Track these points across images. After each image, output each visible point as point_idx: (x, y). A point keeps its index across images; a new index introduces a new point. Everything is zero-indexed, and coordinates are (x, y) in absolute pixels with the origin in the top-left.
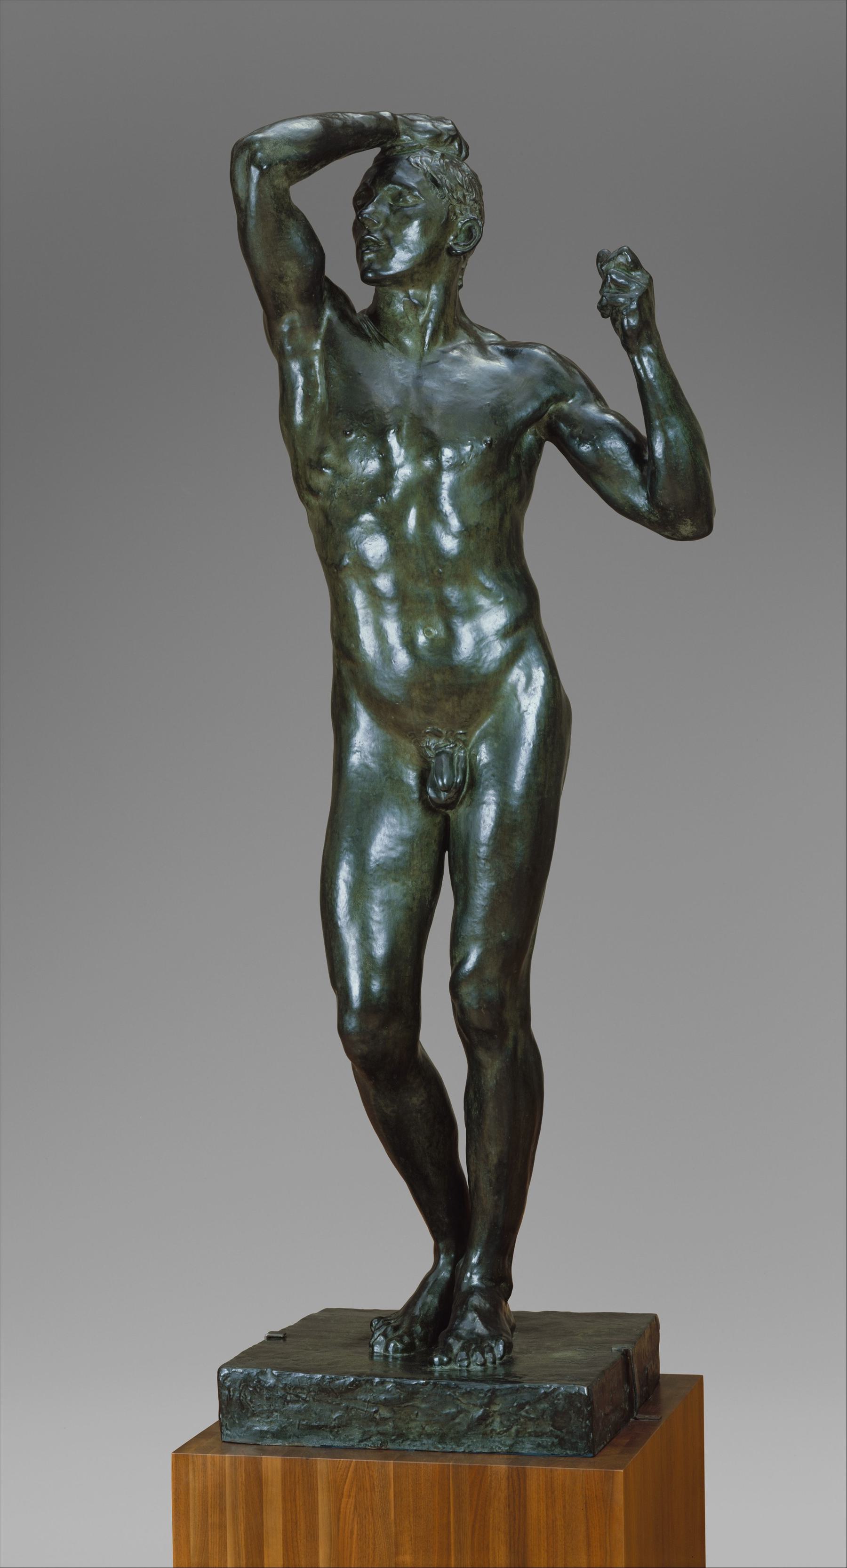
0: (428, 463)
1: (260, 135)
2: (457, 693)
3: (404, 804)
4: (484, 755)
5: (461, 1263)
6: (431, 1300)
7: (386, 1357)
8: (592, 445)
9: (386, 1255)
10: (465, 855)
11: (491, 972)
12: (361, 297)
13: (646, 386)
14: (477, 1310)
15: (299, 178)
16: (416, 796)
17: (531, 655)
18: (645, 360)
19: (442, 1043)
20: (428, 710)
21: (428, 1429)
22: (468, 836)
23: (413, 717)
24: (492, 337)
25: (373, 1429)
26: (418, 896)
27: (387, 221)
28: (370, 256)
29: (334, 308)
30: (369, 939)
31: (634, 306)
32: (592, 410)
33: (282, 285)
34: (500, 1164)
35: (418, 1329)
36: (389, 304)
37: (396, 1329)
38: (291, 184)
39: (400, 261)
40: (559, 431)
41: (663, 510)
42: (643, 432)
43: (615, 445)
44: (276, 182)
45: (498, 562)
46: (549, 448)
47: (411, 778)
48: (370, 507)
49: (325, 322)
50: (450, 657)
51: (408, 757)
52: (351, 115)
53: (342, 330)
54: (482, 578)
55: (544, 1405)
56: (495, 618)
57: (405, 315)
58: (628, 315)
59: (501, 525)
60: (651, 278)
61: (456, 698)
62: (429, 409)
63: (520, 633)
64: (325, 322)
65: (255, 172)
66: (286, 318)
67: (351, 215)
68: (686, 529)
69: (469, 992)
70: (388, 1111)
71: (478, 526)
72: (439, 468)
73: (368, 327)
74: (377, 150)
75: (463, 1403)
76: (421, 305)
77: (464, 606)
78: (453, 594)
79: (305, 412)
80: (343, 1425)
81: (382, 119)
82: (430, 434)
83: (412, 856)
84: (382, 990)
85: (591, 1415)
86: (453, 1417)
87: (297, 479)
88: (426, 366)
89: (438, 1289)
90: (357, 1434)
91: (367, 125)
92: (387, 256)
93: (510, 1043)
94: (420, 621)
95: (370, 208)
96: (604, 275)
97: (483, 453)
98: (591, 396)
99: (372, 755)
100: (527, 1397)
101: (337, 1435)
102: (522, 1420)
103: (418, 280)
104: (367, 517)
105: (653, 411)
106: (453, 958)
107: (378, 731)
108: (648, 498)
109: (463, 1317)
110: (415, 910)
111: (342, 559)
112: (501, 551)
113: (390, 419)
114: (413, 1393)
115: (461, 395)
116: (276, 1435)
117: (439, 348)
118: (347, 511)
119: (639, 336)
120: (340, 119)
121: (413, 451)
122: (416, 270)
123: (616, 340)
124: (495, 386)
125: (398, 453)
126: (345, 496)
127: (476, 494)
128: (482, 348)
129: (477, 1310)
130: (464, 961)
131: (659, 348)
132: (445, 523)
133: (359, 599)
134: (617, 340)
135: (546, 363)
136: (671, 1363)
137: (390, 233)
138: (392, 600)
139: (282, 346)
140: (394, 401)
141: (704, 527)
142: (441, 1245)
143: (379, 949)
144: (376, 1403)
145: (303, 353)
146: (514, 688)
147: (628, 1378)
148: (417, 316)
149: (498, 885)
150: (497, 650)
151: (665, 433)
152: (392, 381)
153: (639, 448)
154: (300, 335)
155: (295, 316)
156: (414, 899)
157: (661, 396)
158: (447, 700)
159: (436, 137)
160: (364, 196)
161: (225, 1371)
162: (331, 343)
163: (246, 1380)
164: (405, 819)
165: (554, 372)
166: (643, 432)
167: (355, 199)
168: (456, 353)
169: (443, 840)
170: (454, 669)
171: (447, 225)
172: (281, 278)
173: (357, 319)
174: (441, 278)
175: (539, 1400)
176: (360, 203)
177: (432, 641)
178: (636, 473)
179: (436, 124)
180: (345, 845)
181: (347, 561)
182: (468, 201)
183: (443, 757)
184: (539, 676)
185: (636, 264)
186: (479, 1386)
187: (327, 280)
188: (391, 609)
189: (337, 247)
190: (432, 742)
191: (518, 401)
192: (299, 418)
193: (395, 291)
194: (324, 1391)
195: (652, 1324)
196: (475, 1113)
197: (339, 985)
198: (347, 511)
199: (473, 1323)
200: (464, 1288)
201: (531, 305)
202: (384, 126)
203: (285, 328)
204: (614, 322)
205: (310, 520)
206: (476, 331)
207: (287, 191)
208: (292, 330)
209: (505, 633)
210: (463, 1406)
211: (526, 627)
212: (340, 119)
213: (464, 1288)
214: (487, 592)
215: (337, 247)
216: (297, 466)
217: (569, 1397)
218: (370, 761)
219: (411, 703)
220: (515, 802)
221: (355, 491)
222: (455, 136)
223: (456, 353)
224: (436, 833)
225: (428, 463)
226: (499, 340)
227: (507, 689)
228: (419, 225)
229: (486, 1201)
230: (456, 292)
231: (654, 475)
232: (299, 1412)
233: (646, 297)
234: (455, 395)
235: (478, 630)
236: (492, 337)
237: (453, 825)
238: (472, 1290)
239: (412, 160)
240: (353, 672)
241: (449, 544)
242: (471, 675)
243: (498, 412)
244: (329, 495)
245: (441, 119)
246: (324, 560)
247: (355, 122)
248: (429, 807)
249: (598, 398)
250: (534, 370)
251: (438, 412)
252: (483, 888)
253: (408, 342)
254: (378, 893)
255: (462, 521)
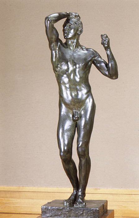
0: (75, 67)
1: (49, 16)
2: (78, 103)
3: (70, 120)
4: (82, 113)
5: (78, 192)
6: (73, 197)
7: (66, 206)
8: (100, 64)
10: (79, 128)
11: (83, 146)
12: (64, 41)
13: (108, 56)
14: (80, 198)
15: (55, 23)
16: (72, 119)
17: (90, 97)
18: (108, 51)
19: (75, 158)
20: (74, 105)
21: (74, 215)
22: (80, 125)
23: (72, 106)
25: (65, 215)
27: (68, 29)
28: (65, 35)
29: (60, 43)
30: (64, 141)
31: (107, 43)
32: (100, 59)
34: (84, 176)
35: (71, 201)
36: (68, 42)
37: (68, 201)
38: (54, 23)
39: (70, 36)
40: (94, 62)
41: (111, 75)
42: (108, 63)
43: (103, 64)
45: (85, 82)
46: (93, 64)
47: (71, 116)
48: (66, 74)
49: (59, 45)
50: (78, 97)
51: (71, 113)
53: (61, 46)
54: (83, 85)
55: (91, 211)
56: (84, 91)
57: (71, 44)
58: (106, 45)
59: (86, 77)
60: (109, 39)
61: (78, 104)
62: (75, 59)
63: (88, 94)
64: (59, 45)
65: (49, 22)
66: (53, 44)
67: (62, 28)
68: (114, 78)
69: (80, 149)
70: (67, 168)
71: (82, 77)
72: (76, 68)
73: (65, 45)
74: (66, 18)
75: (79, 211)
76: (74, 42)
77: (80, 89)
78: (78, 87)
79: (55, 59)
80: (61, 215)
81: (67, 13)
82: (75, 62)
83: (71, 128)
84: (67, 149)
85: (99, 213)
86: (78, 213)
87: (54, 69)
88: (74, 52)
89: (74, 196)
90: (63, 216)
92: (68, 35)
93: (86, 157)
94: (73, 92)
95: (66, 27)
96: (102, 38)
97: (83, 66)
98: (99, 57)
99: (65, 112)
100: (89, 210)
101: (60, 216)
104: (65, 75)
105: (109, 59)
106: (77, 144)
107: (66, 109)
108: (108, 73)
109: (78, 199)
111: (61, 82)
112: (85, 81)
113: (69, 60)
114: (72, 210)
116: (50, 216)
117: (76, 49)
118: (62, 74)
119: (107, 48)
121: (72, 65)
123: (104, 48)
125: (70, 66)
126: (61, 72)
127: (82, 72)
128: (83, 49)
129: (80, 198)
130: (79, 144)
131: (110, 50)
132: (77, 76)
133: (63, 88)
134: (104, 48)
135: (93, 52)
136: (109, 208)
137: (69, 31)
138: (69, 88)
139: (52, 49)
140: (69, 57)
141: (117, 77)
142: (74, 189)
143: (66, 143)
144: (66, 211)
145: (55, 50)
146: (87, 102)
147: (104, 209)
148: (73, 44)
149: (85, 133)
150: (85, 96)
151: (111, 63)
152: (69, 54)
153: (107, 65)
154: (55, 47)
155: (54, 44)
157: (110, 57)
159: (76, 16)
160: (64, 26)
161: (42, 207)
162: (59, 48)
163: (46, 208)
164: (70, 122)
165: (94, 53)
166: (108, 63)
167: (63, 26)
168: (78, 50)
169: (76, 126)
170: (78, 99)
171: (77, 30)
172: (52, 38)
173: (63, 44)
174: (76, 38)
175: (91, 210)
176: (64, 26)
177: (75, 95)
178: (106, 69)
180: (61, 126)
181: (62, 82)
183: (76, 113)
184: (91, 100)
185: (107, 37)
186: (82, 209)
187: (59, 39)
188: (68, 90)
189: (61, 33)
190: (74, 110)
191: (88, 57)
192: (54, 60)
193: (69, 40)
194: (58, 210)
195: (107, 201)
196: (80, 168)
197: (60, 148)
198: (62, 74)
199: (80, 200)
200: (78, 195)
201: (90, 41)
203: (52, 46)
204: (103, 45)
205: (56, 76)
207: (53, 25)
208: (53, 46)
209: (86, 94)
211: (89, 93)
213: (78, 195)
214: (83, 87)
215: (61, 33)
217: (95, 210)
218: (65, 114)
219: (71, 104)
220: (87, 120)
221: (63, 71)
222: (78, 16)
223: (78, 50)
224: (75, 125)
225: (75, 67)
227: (86, 102)
229: (82, 182)
231: (109, 69)
232: (54, 213)
233: (108, 42)
235: (82, 93)
237: (77, 123)
238: (80, 195)
240: (62, 99)
241: (78, 79)
242: (81, 100)
243: (85, 59)
244: (59, 72)
245: (76, 13)
246: (58, 82)
248: (74, 120)
249: (101, 57)
250: (90, 52)
251: (76, 59)
252: (82, 133)
253: (71, 48)
254: (66, 134)
255: (80, 76)
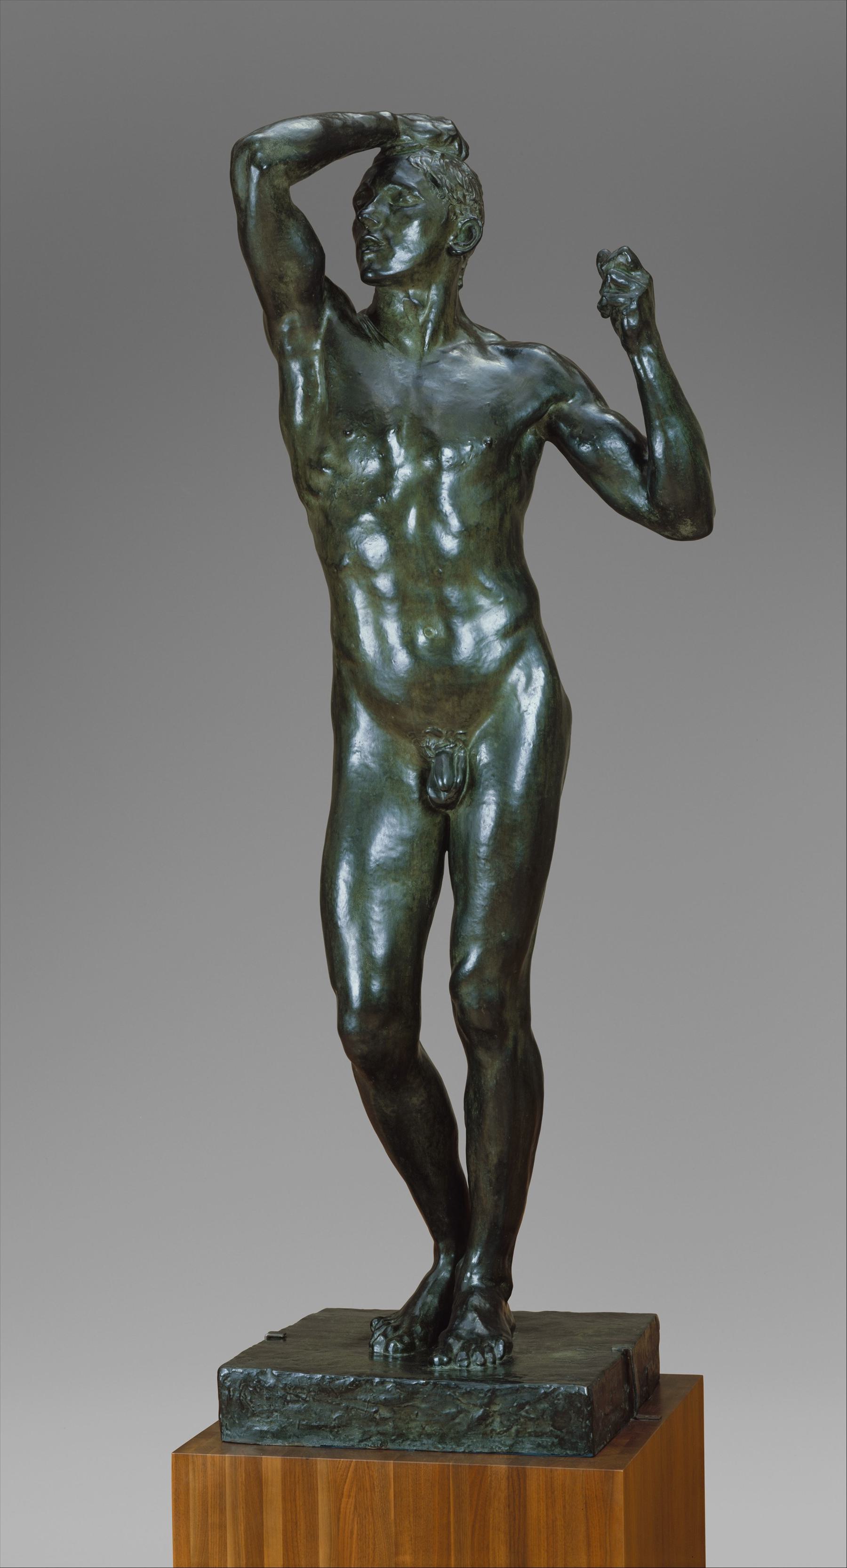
0: (428, 463)
1: (260, 135)
2: (457, 693)
3: (404, 804)
4: (484, 755)
5: (461, 1263)
6: (431, 1300)
7: (386, 1357)
8: (592, 445)
9: (386, 1255)
10: (465, 855)
11: (491, 972)
12: (361, 297)
13: (646, 386)
14: (477, 1310)
15: (299, 178)
16: (416, 796)
17: (531, 655)
18: (645, 360)
19: (442, 1043)
20: (428, 710)
21: (428, 1429)
22: (468, 836)
23: (413, 717)
24: (492, 337)
25: (373, 1429)
26: (418, 896)
27: (387, 221)
28: (370, 256)
29: (334, 308)
30: (369, 939)
31: (634, 306)
32: (592, 410)
33: (282, 285)
34: (500, 1164)
35: (418, 1329)
36: (389, 304)
37: (396, 1329)
38: (291, 184)
39: (400, 261)
40: (559, 431)
41: (663, 510)
42: (643, 432)
43: (615, 445)
44: (276, 182)
45: (498, 562)
46: (549, 448)
47: (411, 778)
48: (370, 507)
49: (325, 322)
50: (450, 657)
51: (408, 757)
52: (351, 115)
53: (342, 330)
54: (482, 578)
55: (544, 1405)
56: (495, 618)
57: (405, 315)
58: (628, 315)
59: (501, 525)
60: (651, 278)
61: (456, 698)
62: (429, 409)
63: (520, 633)
64: (325, 322)
65: (255, 172)
66: (286, 318)
67: (351, 215)
68: (686, 529)
69: (469, 992)
70: (388, 1111)
71: (478, 526)
72: (439, 468)
73: (368, 327)
74: (377, 150)
75: (463, 1403)
76: (421, 305)
77: (464, 606)
78: (453, 594)
79: (305, 412)
80: (343, 1425)
81: (382, 119)
82: (430, 434)
83: (412, 856)
84: (382, 990)
85: (591, 1415)
86: (453, 1417)
87: (297, 479)
88: (426, 366)
89: (438, 1289)
90: (357, 1434)
91: (367, 125)
92: (387, 256)
93: (510, 1043)
94: (420, 621)
95: (370, 208)
96: (604, 275)
97: (483, 453)
98: (591, 396)
99: (372, 755)
100: (527, 1397)
101: (337, 1435)
102: (522, 1420)
103: (418, 280)
104: (367, 517)
105: (653, 411)
106: (453, 958)
107: (378, 731)
108: (648, 498)
109: (463, 1317)
110: (415, 910)
111: (342, 559)
112: (501, 551)
113: (390, 419)
114: (413, 1393)
115: (461, 395)
116: (276, 1435)
117: (439, 348)
118: (347, 511)
119: (639, 336)
120: (340, 119)
121: (413, 451)
122: (416, 270)
123: (616, 340)
124: (495, 386)
125: (398, 453)
126: (345, 496)
127: (476, 494)
128: (482, 348)
129: (477, 1310)
130: (464, 961)
131: (659, 348)
132: (445, 523)
133: (359, 599)
134: (617, 340)
135: (546, 363)
136: (671, 1363)
137: (390, 233)
138: (392, 600)
139: (282, 346)
140: (394, 401)
141: (704, 527)
142: (441, 1245)
143: (379, 949)
144: (376, 1403)
145: (303, 353)
146: (514, 688)
147: (628, 1378)
148: (417, 316)
149: (498, 885)
150: (497, 650)
151: (665, 433)
152: (392, 381)
153: (639, 448)
154: (300, 335)
155: (295, 316)
156: (414, 899)
157: (661, 396)
158: (447, 700)
159: (436, 137)
160: (364, 196)
161: (225, 1371)
162: (331, 343)
163: (246, 1380)
164: (405, 819)
165: (554, 372)
166: (643, 432)
167: (355, 199)
168: (456, 353)
169: (443, 840)
170: (454, 669)
171: (447, 225)
172: (281, 278)
173: (357, 319)
174: (441, 278)
175: (539, 1400)
176: (360, 203)
177: (432, 641)
178: (636, 473)
179: (436, 124)
180: (345, 845)
181: (347, 561)
182: (468, 201)
183: (443, 757)
184: (539, 676)
185: (636, 264)
186: (479, 1386)
187: (327, 280)
188: (391, 609)
189: (337, 247)
190: (432, 742)
191: (518, 401)
192: (299, 418)
193: (395, 291)
194: (324, 1391)
195: (652, 1324)
196: (475, 1113)
197: (339, 985)
198: (347, 511)
199: (473, 1323)
200: (464, 1288)
201: (531, 305)
202: (384, 126)
203: (285, 328)
204: (614, 322)
205: (310, 520)
206: (476, 331)
207: (287, 191)
208: (292, 330)
209: (505, 633)
210: (463, 1406)
211: (526, 627)
212: (340, 119)
213: (464, 1288)
214: (487, 592)
215: (337, 247)
216: (297, 466)
217: (569, 1397)
218: (370, 761)
219: (411, 703)
220: (515, 802)
221: (355, 491)
222: (455, 136)
223: (456, 353)
224: (436, 833)
225: (428, 463)
226: (499, 340)
227: (507, 689)
228: (419, 225)
229: (486, 1201)
230: (456, 292)
231: (654, 475)
232: (299, 1412)
233: (646, 297)
234: (455, 395)
235: (478, 630)
236: (492, 337)
237: (453, 825)
238: (472, 1290)
239: (412, 160)
240: (353, 672)
241: (449, 544)
242: (471, 675)
243: (498, 412)
244: (329, 495)
245: (441, 119)
246: (324, 560)
247: (355, 122)
248: (429, 807)
249: (598, 398)
250: (534, 370)
251: (438, 412)
252: (483, 888)
253: (408, 342)
254: (378, 893)
255: (462, 521)
